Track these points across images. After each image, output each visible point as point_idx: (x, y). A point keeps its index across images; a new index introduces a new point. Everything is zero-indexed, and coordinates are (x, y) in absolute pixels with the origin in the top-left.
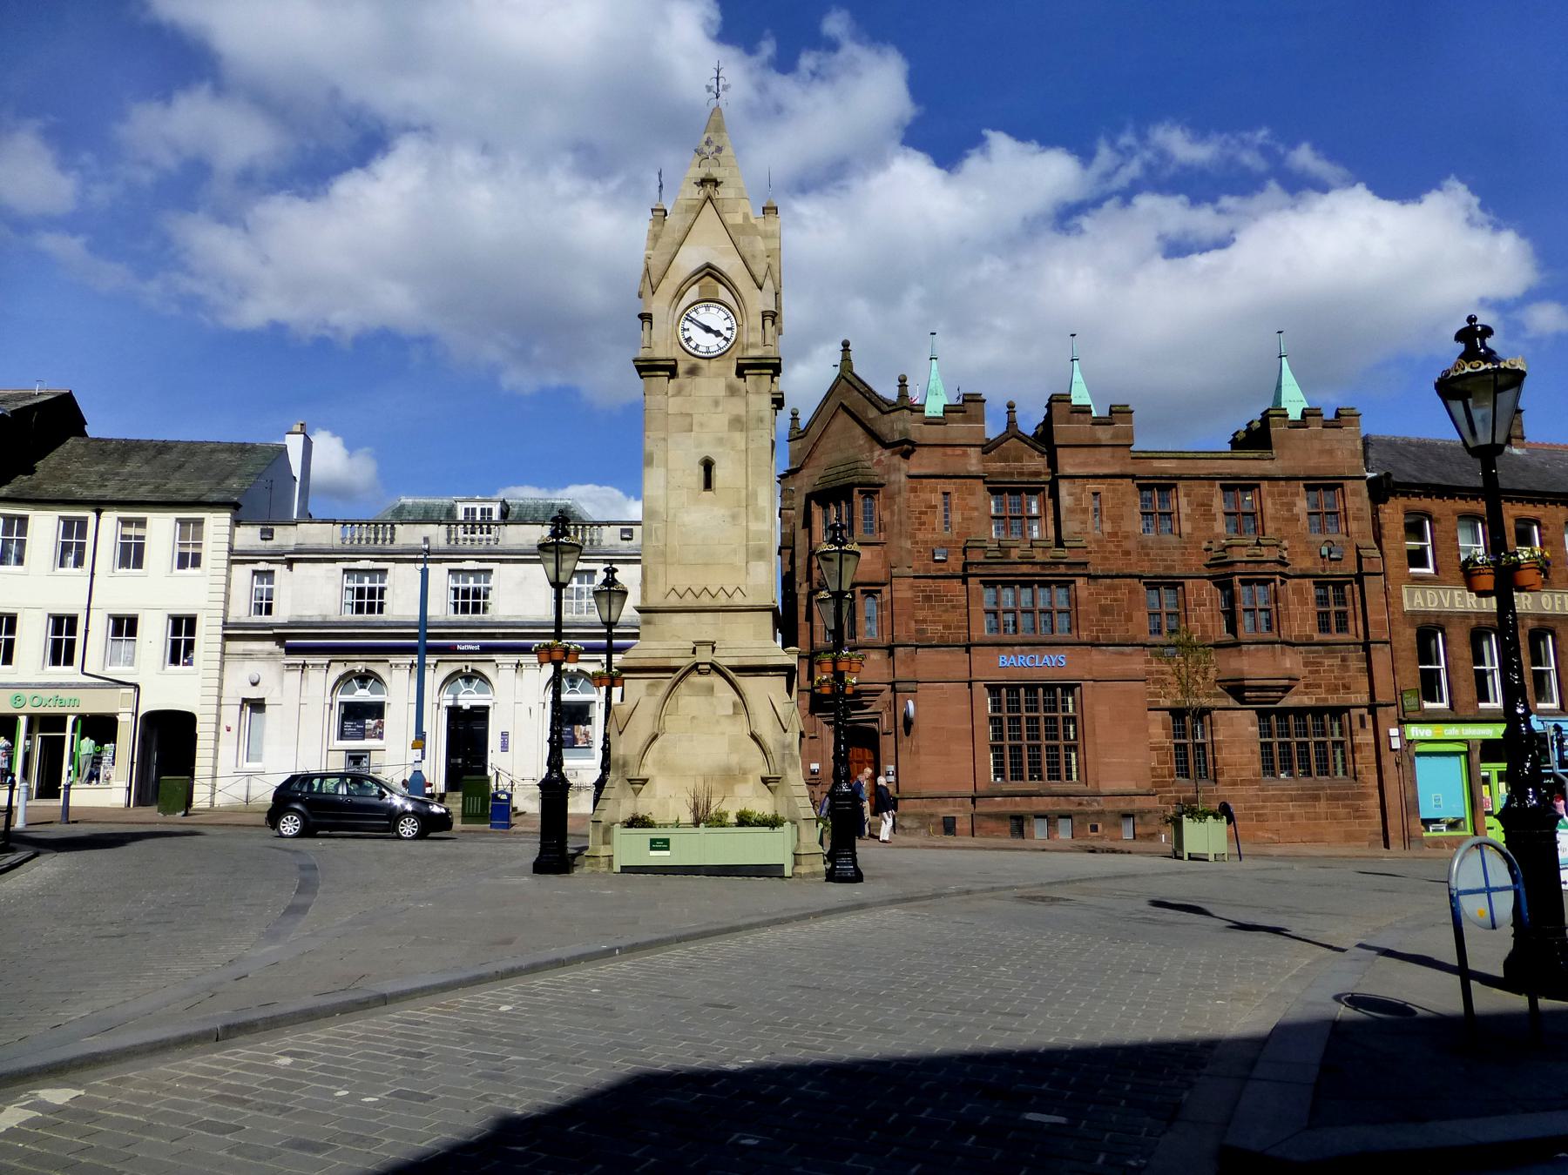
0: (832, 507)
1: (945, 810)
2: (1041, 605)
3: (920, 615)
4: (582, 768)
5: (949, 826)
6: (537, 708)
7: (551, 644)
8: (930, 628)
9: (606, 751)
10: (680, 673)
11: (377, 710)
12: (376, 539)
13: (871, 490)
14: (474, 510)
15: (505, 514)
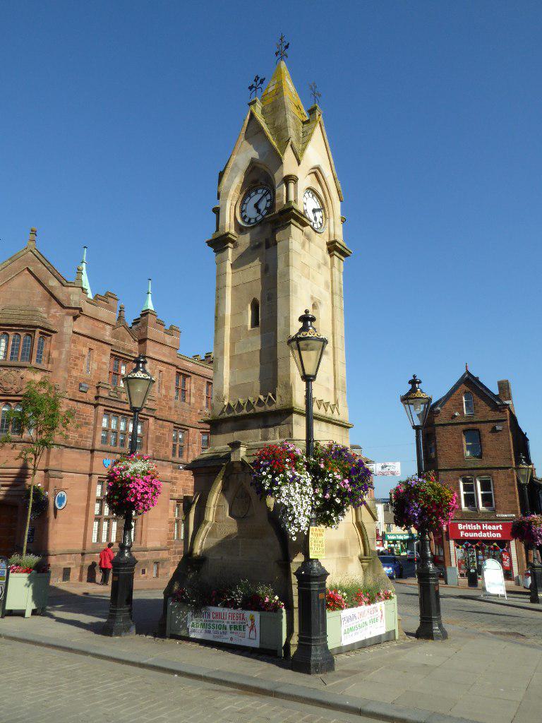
2: (113, 427)
13: (47, 332)
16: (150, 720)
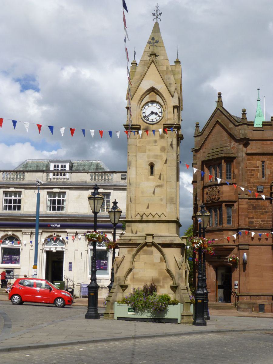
0: (212, 169)
1: (260, 302)
3: (251, 215)
4: (104, 279)
5: (261, 308)
6: (84, 253)
7: (90, 225)
8: (255, 221)
9: (112, 274)
10: (140, 246)
11: (17, 252)
12: (17, 178)
13: (230, 160)
14: (58, 166)
15: (71, 167)
16: (255, 363)
